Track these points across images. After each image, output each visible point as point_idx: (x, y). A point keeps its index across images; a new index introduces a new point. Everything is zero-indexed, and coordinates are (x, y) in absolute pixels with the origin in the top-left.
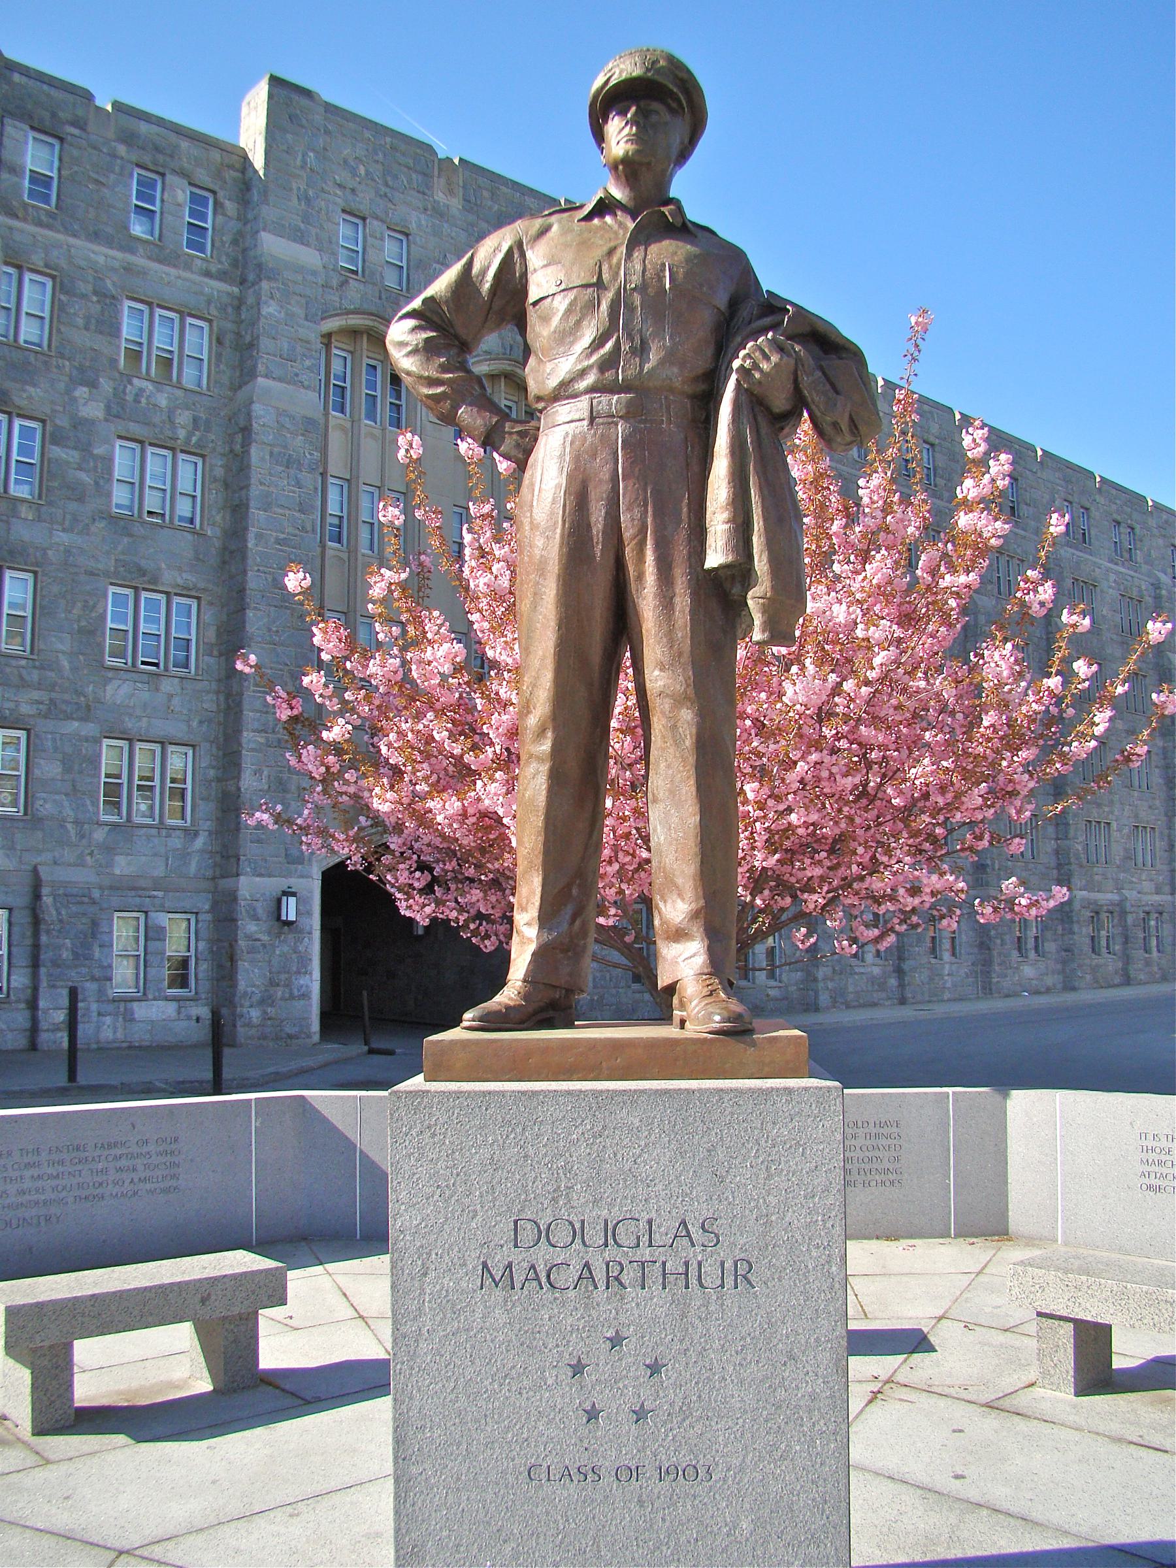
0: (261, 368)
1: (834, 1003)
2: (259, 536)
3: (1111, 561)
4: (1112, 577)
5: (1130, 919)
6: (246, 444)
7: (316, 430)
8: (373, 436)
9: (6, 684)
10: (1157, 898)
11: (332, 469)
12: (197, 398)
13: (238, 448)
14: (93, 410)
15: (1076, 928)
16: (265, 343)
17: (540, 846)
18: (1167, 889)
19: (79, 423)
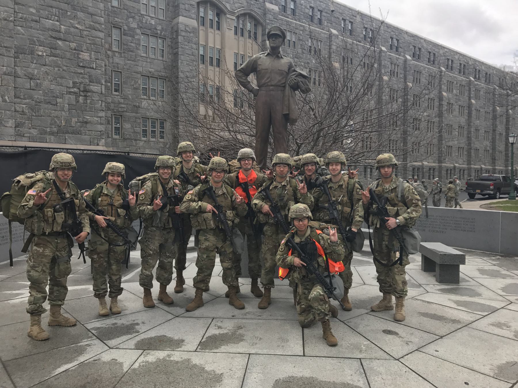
0: (180, 13)
1: (396, 192)
2: (181, 63)
3: (427, 65)
4: (427, 69)
5: (424, 170)
6: (177, 36)
7: (195, 31)
8: (212, 32)
9: (2, 47)
10: (434, 164)
11: (201, 43)
12: (162, 21)
13: (174, 36)
14: (134, 25)
15: (408, 172)
16: (181, 6)
17: (371, 296)
18: (437, 162)
19: (130, 29)
